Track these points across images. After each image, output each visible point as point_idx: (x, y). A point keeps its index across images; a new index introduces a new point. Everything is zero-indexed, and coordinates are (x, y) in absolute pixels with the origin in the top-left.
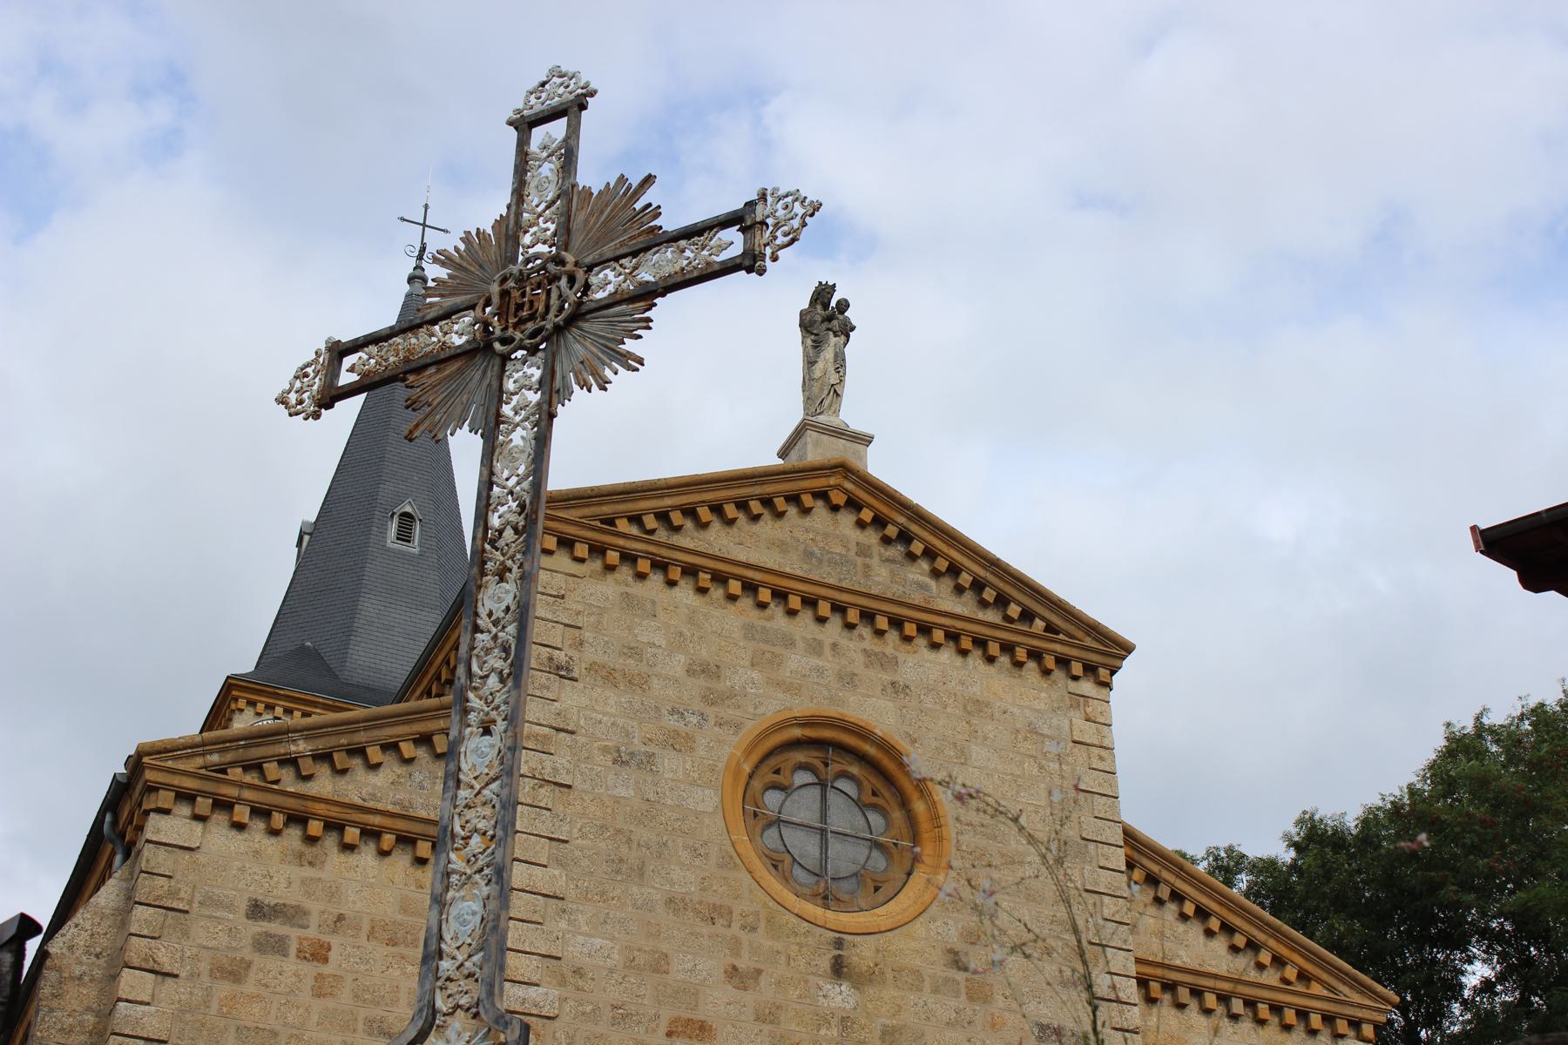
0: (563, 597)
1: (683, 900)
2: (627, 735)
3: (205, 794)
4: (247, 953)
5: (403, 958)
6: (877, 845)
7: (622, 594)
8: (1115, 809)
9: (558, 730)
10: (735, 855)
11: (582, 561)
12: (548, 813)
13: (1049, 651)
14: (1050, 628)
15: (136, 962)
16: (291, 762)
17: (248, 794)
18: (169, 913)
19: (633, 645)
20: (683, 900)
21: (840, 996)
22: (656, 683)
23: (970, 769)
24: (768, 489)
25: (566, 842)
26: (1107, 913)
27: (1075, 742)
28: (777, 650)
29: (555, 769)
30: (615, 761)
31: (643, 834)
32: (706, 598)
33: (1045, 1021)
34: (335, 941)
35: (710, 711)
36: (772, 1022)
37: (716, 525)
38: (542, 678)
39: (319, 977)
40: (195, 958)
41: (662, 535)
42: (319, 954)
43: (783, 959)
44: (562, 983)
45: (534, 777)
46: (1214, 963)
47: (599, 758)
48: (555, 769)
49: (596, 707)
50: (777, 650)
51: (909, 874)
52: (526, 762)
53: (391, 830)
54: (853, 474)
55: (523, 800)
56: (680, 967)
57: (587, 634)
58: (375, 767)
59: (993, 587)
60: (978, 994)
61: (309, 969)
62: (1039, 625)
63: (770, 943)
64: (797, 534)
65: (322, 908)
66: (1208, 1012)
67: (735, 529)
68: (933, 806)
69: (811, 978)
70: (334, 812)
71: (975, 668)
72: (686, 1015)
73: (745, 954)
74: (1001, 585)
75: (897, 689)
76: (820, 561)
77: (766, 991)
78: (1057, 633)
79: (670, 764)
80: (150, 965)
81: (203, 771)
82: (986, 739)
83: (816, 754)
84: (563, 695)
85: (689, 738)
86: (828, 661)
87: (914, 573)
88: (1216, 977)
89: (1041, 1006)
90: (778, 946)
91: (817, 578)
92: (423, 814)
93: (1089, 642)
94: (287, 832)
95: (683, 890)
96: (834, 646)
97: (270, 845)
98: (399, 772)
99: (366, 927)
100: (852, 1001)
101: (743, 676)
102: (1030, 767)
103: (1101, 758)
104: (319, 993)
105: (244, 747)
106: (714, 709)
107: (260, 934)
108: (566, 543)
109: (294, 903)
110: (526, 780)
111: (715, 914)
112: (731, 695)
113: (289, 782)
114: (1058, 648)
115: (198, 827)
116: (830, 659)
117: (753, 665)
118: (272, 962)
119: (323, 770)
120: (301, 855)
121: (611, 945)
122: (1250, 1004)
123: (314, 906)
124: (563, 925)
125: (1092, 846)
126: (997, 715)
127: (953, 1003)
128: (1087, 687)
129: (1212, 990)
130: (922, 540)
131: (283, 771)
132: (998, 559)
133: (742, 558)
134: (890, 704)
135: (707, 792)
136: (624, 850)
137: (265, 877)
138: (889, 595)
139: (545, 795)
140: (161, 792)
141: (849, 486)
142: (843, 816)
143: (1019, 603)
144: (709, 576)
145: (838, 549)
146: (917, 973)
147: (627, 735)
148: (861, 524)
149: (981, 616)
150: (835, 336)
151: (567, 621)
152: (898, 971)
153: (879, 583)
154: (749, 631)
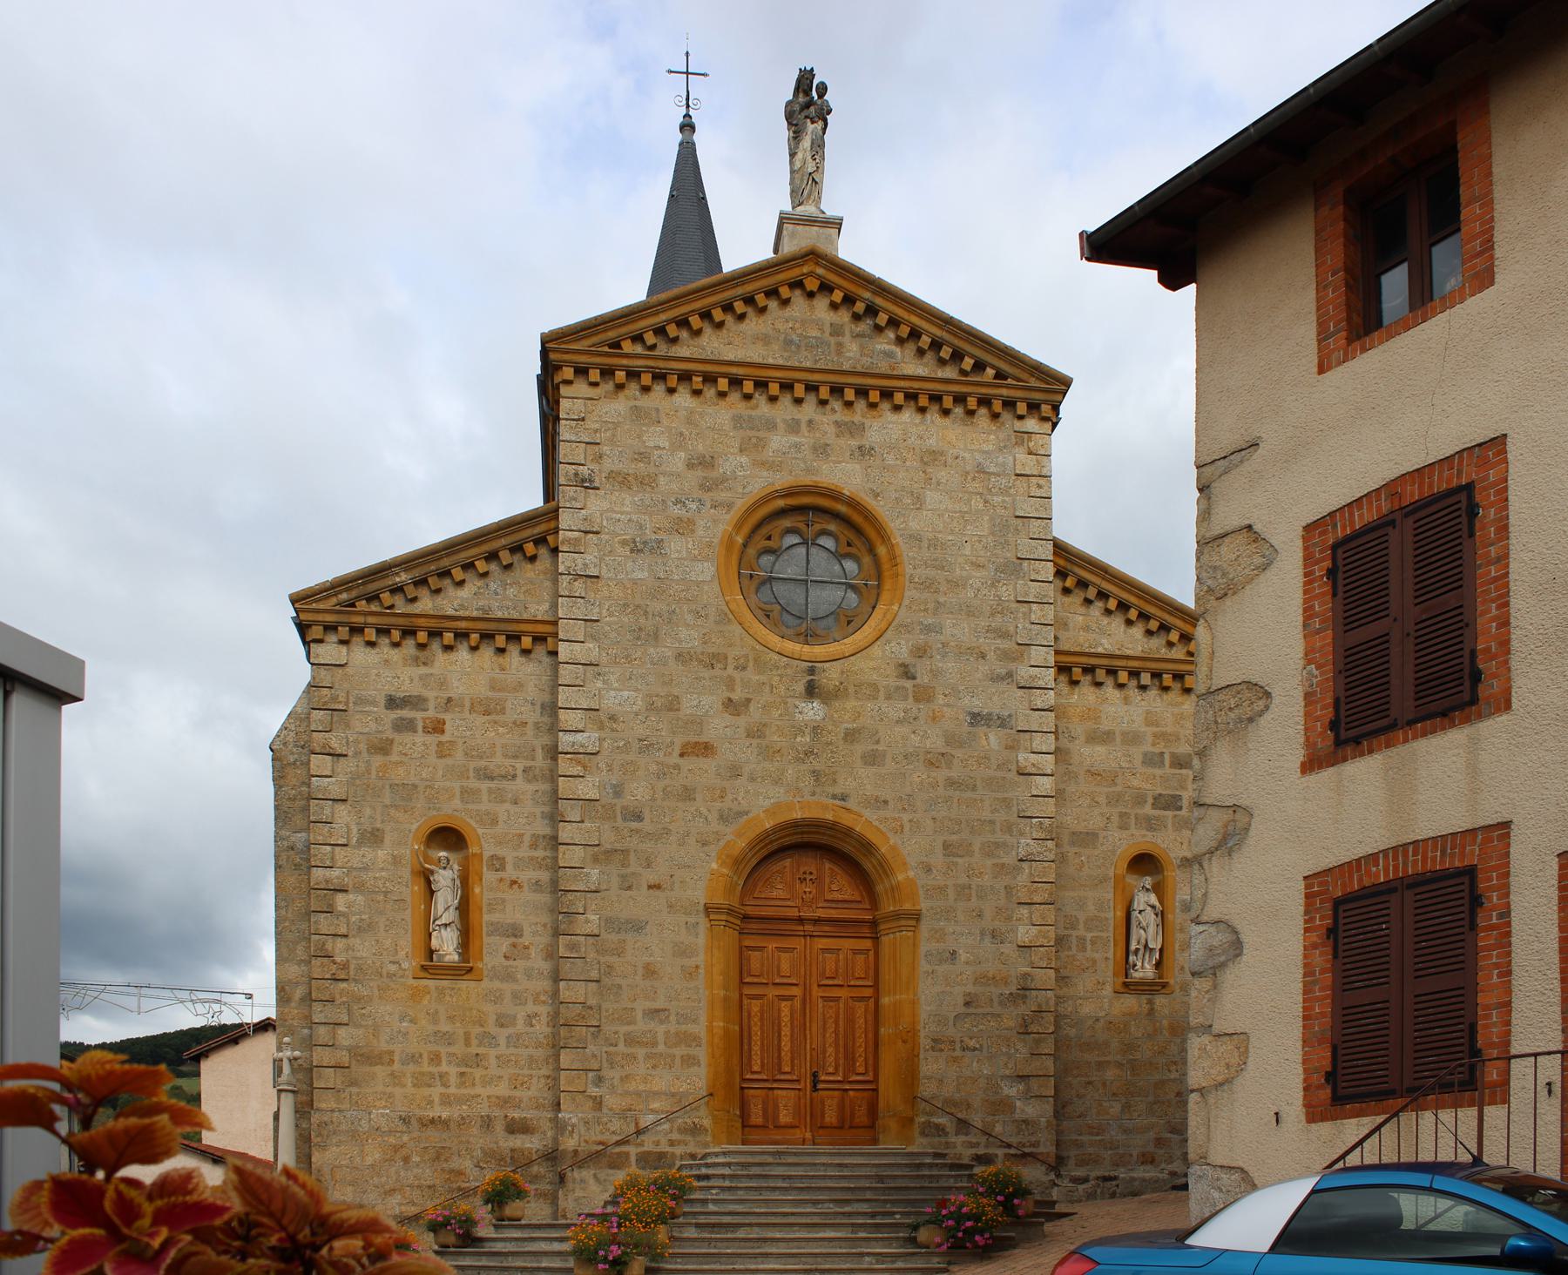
0: (583, 419)
1: (689, 653)
2: (641, 528)
3: (343, 624)
4: (389, 734)
5: (495, 723)
6: (853, 587)
7: (631, 408)
8: (1048, 528)
9: (586, 532)
10: (729, 612)
11: (595, 384)
12: (582, 601)
13: (996, 397)
14: (1000, 375)
15: (318, 750)
16: (397, 590)
17: (371, 620)
18: (335, 713)
19: (642, 450)
20: (689, 653)
21: (813, 711)
22: (662, 480)
23: (925, 513)
24: (749, 288)
25: (597, 621)
26: (1033, 618)
27: (1017, 475)
28: (761, 434)
29: (585, 565)
30: (632, 551)
31: (656, 606)
32: (702, 398)
33: (976, 710)
34: (447, 717)
35: (707, 497)
36: (759, 737)
37: (708, 330)
38: (571, 491)
39: (440, 744)
40: (357, 742)
41: (662, 349)
42: (437, 727)
43: (767, 689)
44: (601, 728)
45: (569, 574)
46: (1130, 646)
47: (620, 550)
48: (585, 565)
49: (616, 509)
50: (761, 434)
51: (874, 607)
52: (563, 562)
53: (475, 631)
54: (823, 259)
55: (563, 593)
56: (689, 705)
57: (605, 448)
58: (461, 583)
59: (950, 344)
60: (924, 695)
61: (432, 739)
62: (990, 372)
63: (757, 678)
64: (779, 326)
65: (436, 695)
66: (1121, 686)
67: (725, 331)
68: (892, 548)
69: (789, 700)
70: (432, 623)
71: (932, 422)
72: (696, 739)
73: (738, 689)
74: (956, 342)
75: (864, 452)
76: (799, 347)
77: (755, 713)
78: (1005, 378)
79: (676, 546)
80: (328, 750)
81: (338, 608)
82: (938, 484)
83: (801, 518)
84: (588, 503)
85: (691, 522)
86: (805, 437)
87: (882, 343)
88: (1128, 658)
89: (974, 699)
90: (763, 678)
91: (797, 364)
92: (499, 615)
93: (1034, 383)
94: (404, 642)
95: (689, 645)
96: (810, 422)
97: (395, 655)
98: (479, 584)
99: (467, 704)
100: (821, 714)
101: (734, 463)
102: (977, 503)
103: (1039, 486)
104: (441, 756)
105: (363, 584)
106: (710, 494)
107: (396, 719)
108: (581, 371)
109: (416, 694)
110: (564, 577)
111: (714, 660)
112: (724, 479)
113: (401, 607)
114: (1004, 392)
115: (344, 649)
116: (806, 434)
117: (741, 451)
118: (407, 738)
119: (424, 592)
120: (417, 659)
121: (636, 694)
122: (1157, 675)
123: (430, 695)
124: (599, 685)
125: (1025, 563)
126: (949, 461)
127: (901, 705)
128: (1031, 424)
129: (1124, 668)
130: (886, 311)
131: (396, 598)
132: (952, 318)
133: (731, 357)
134: (857, 466)
135: (705, 564)
136: (642, 620)
137: (394, 678)
138: (859, 369)
139: (579, 587)
140: (314, 627)
141: (820, 271)
142: (822, 564)
143: (972, 356)
144: (700, 379)
145: (815, 333)
146: (874, 687)
147: (641, 528)
148: (834, 306)
149: (940, 374)
150: (813, 123)
151: (587, 440)
152: (858, 686)
153: (850, 358)
154: (737, 421)
